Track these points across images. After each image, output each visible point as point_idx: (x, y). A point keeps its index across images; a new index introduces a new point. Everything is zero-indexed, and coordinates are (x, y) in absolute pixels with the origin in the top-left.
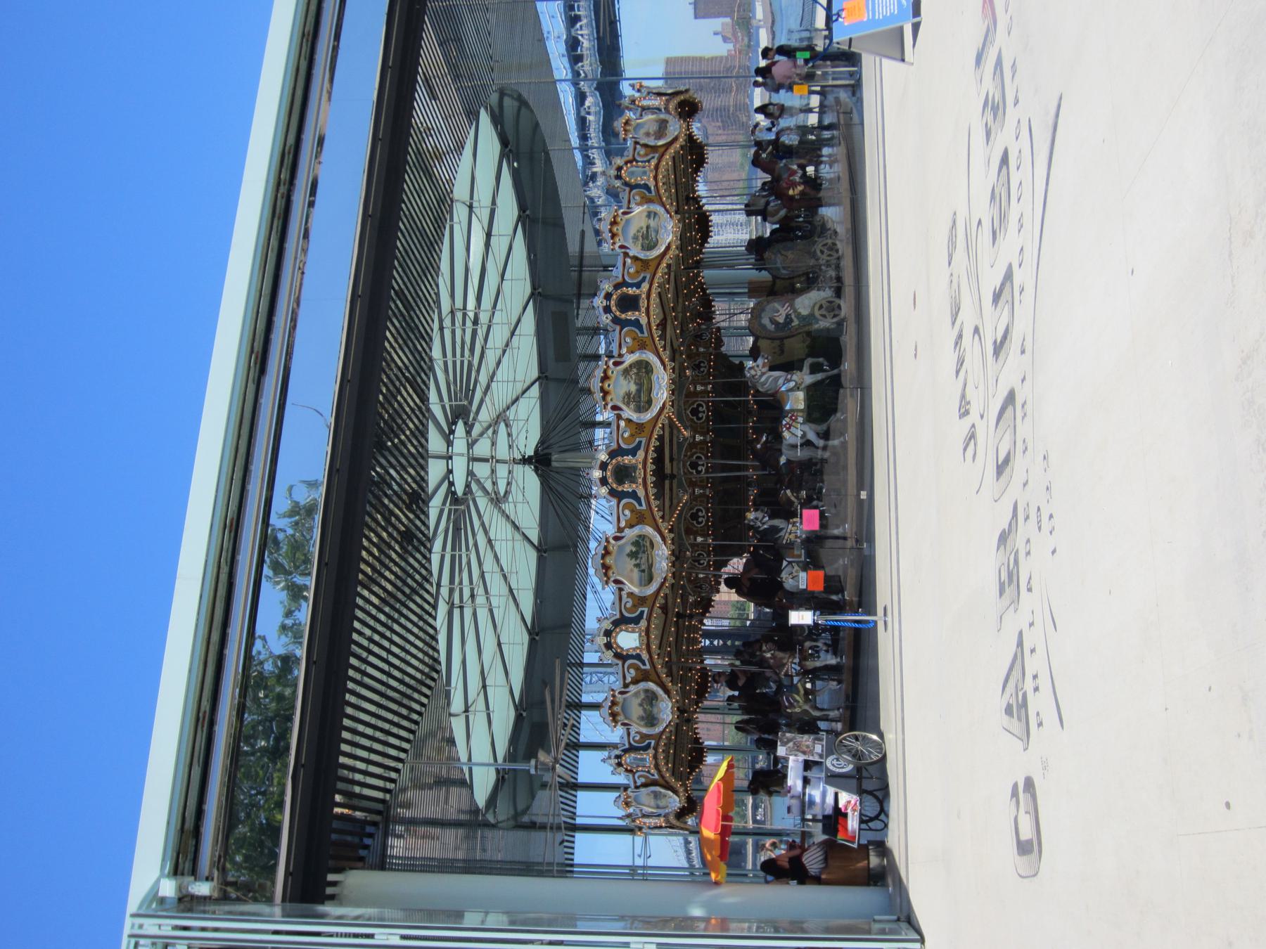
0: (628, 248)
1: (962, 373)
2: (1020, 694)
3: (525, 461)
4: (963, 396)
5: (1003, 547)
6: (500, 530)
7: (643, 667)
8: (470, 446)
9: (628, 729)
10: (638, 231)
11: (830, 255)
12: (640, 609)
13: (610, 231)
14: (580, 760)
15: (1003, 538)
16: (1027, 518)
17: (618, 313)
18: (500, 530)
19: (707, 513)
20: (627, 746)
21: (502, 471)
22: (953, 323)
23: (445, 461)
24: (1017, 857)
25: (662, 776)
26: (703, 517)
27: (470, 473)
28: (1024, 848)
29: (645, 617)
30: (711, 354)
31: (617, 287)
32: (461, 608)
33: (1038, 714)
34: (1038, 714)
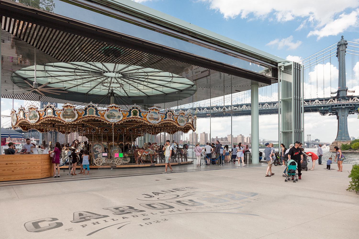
2: (88, 218)
5: (129, 208)
6: (93, 84)
10: (113, 114)
11: (116, 162)
14: (10, 99)
15: (131, 208)
17: (132, 110)
18: (93, 84)
19: (107, 133)
21: (109, 85)
23: (113, 71)
27: (109, 77)
28: (36, 225)
29: (98, 116)
30: (135, 134)
31: (139, 110)
32: (74, 72)
33: (86, 225)
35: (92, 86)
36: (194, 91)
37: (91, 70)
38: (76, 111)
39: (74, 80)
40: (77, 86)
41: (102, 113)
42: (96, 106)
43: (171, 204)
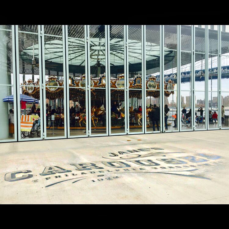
0: (118, 80)
1: (128, 152)
2: (55, 172)
3: (98, 62)
4: (124, 153)
8: (101, 50)
13: (152, 78)
15: (94, 165)
16: (100, 172)
21: (96, 57)
22: (139, 149)
24: (11, 173)
27: (96, 50)
28: (13, 175)
33: (50, 178)
34: (50, 178)
35: (83, 59)
36: (172, 57)
40: (71, 59)
43: (129, 163)
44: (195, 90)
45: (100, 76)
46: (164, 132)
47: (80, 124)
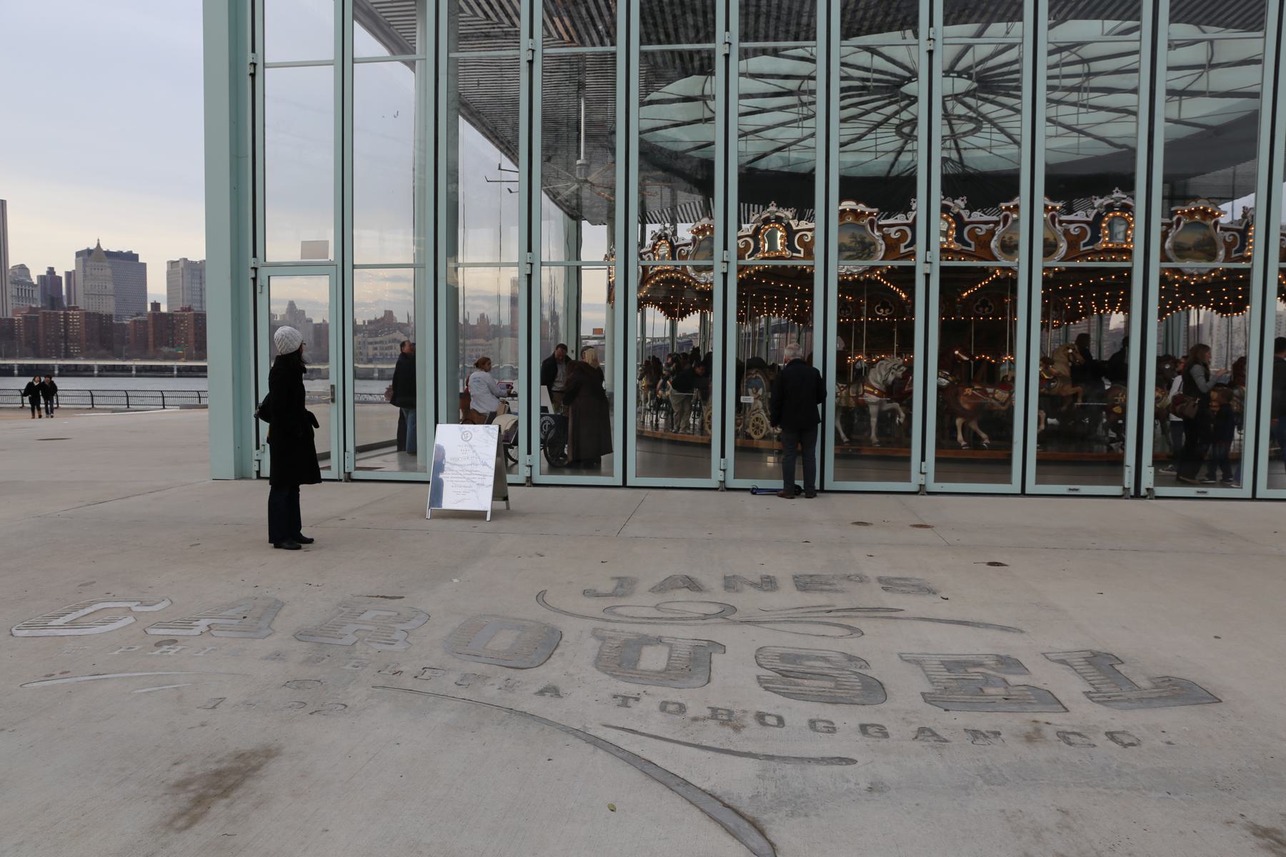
7: (902, 245)
9: (690, 244)
12: (802, 250)
20: (675, 244)
25: (651, 277)
26: (884, 313)
29: (794, 254)
37: (877, 76)
38: (879, 230)
39: (795, 121)
41: (980, 234)
42: (789, 219)
44: (470, 259)
45: (958, 201)
46: (1143, 492)
47: (960, 437)
